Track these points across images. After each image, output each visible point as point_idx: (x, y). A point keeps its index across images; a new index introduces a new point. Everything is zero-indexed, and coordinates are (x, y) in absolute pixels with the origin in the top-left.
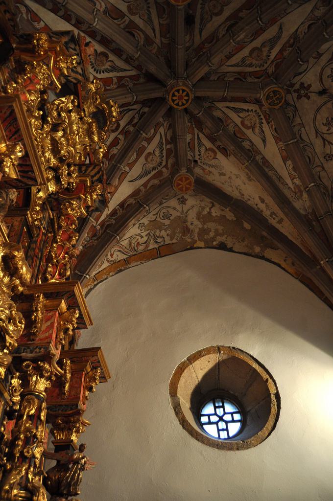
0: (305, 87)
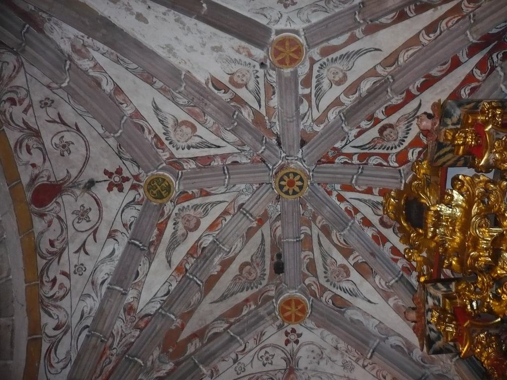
0: (116, 186)
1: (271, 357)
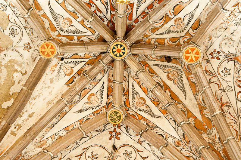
0: (117, 135)
1: (226, 70)
